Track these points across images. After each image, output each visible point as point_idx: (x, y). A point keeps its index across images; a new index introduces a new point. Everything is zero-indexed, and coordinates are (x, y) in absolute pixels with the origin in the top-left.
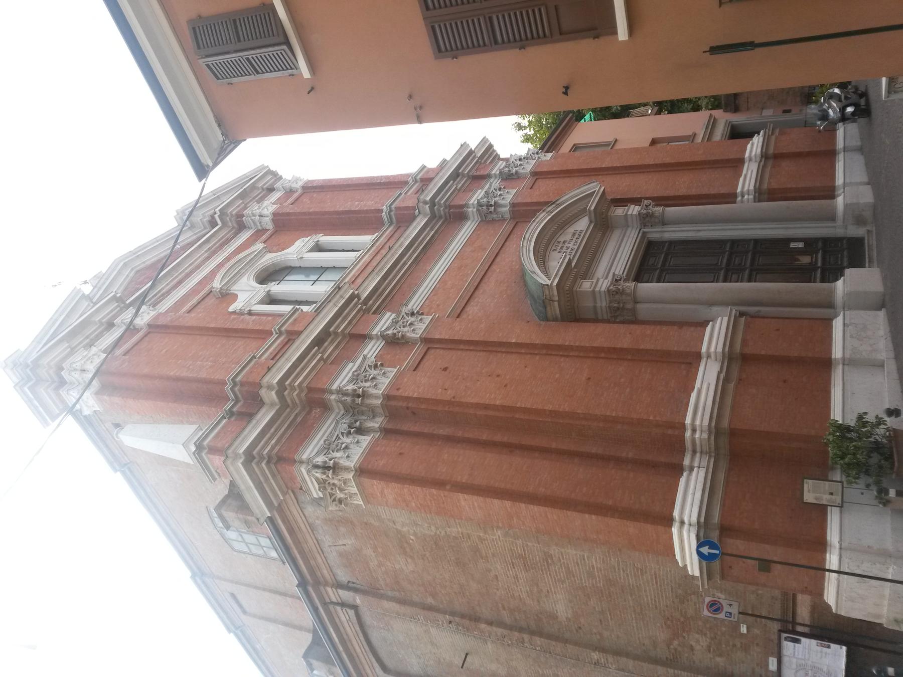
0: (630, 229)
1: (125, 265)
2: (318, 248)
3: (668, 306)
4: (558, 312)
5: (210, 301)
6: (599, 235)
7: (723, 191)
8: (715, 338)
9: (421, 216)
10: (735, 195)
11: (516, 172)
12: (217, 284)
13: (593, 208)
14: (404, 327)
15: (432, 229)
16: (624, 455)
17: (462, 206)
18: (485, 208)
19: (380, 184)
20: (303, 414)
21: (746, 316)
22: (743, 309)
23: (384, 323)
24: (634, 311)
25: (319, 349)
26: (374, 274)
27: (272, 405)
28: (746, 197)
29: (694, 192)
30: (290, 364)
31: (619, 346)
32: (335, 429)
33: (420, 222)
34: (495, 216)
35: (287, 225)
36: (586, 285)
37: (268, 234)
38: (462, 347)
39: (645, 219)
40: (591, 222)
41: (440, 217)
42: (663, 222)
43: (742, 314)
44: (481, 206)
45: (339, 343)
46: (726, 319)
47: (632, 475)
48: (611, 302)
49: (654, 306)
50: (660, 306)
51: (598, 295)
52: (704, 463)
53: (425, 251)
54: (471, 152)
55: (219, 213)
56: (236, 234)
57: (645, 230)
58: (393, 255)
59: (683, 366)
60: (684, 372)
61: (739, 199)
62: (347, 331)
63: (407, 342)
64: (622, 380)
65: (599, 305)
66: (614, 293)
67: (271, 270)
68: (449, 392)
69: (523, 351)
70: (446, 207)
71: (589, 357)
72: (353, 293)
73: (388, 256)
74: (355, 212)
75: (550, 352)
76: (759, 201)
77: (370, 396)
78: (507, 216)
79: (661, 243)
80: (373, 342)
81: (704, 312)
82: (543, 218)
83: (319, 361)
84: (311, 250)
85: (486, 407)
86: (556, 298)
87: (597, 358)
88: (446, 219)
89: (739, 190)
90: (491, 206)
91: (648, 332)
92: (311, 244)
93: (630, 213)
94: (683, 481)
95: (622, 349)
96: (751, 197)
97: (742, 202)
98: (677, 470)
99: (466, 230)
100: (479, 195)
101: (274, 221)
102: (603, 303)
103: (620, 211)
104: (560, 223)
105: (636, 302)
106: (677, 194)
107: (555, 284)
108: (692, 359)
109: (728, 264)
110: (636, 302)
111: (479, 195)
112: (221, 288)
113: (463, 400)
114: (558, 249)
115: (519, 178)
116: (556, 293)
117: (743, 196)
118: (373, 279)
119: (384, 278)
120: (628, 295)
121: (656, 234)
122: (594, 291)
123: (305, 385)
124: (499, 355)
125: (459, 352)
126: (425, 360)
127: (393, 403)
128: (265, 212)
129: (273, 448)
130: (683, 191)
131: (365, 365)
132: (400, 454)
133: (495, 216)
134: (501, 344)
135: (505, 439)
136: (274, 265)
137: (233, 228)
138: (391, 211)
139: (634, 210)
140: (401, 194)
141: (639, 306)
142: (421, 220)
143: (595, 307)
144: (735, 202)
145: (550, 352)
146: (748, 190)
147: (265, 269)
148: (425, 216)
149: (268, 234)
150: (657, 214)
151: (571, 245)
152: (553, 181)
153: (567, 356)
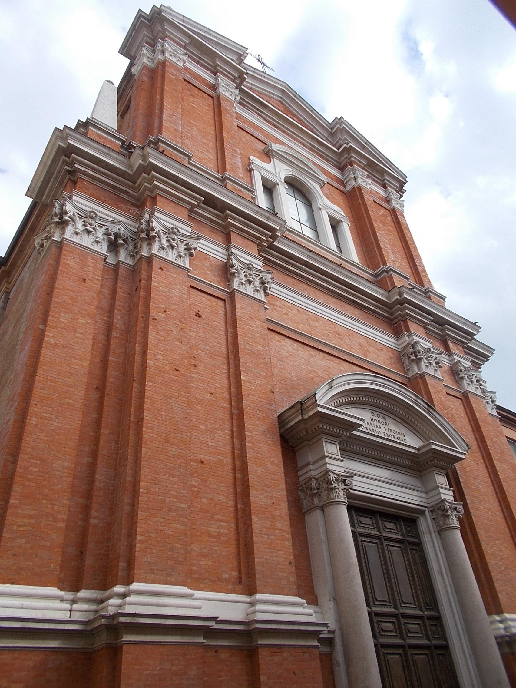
0: (424, 495)
1: (283, 92)
2: (335, 225)
3: (324, 547)
4: (292, 423)
5: (261, 147)
6: (407, 462)
7: (502, 597)
8: (280, 607)
9: (386, 293)
10: (500, 612)
11: (462, 378)
12: (275, 147)
13: (433, 447)
14: (246, 276)
15: (376, 306)
16: (94, 513)
17: (408, 330)
18: (412, 350)
19: (415, 266)
20: (132, 200)
21: (324, 648)
22: (338, 642)
23: (245, 256)
24: (312, 509)
25: (204, 203)
26: (308, 253)
27: (130, 167)
28: (502, 626)
29: (491, 562)
30: (177, 174)
31: (252, 492)
32: (111, 222)
33: (379, 293)
34: (407, 363)
35: (353, 199)
36: (331, 449)
37: (341, 188)
38: (230, 330)
39: (439, 510)
40: (418, 449)
41: (392, 314)
42: (440, 532)
43: (330, 642)
44: (413, 346)
45: (217, 223)
46: (312, 619)
47: (62, 525)
48: (316, 479)
49: (322, 530)
50: (323, 537)
51: (321, 463)
52: (77, 617)
53: (346, 295)
54: (472, 335)
55: (348, 146)
56: (336, 166)
57: (427, 512)
58: (334, 270)
59: (235, 574)
60: (225, 576)
61: (497, 618)
62: (232, 229)
63: (229, 281)
64: (204, 500)
65: (311, 467)
66: (325, 481)
67: (304, 190)
68: (163, 315)
69: (233, 389)
70: (402, 316)
71: (234, 461)
72: (276, 230)
73: (332, 265)
74: (376, 237)
75: (235, 417)
76: (499, 644)
77: (150, 245)
78: (410, 375)
79: (417, 534)
80: (224, 252)
81: (324, 592)
82: (407, 397)
83: (190, 203)
84: (331, 218)
85: (145, 353)
86: (306, 417)
87: (234, 469)
88: (392, 320)
89: (507, 615)
90: (416, 356)
91: (279, 525)
92: (337, 217)
93: (441, 490)
94: (54, 591)
95: (248, 495)
96: (503, 632)
97: (492, 623)
98: (73, 582)
99: (386, 339)
100: (424, 344)
101: (354, 189)
102: (314, 471)
103: (441, 480)
104: (405, 416)
105: (322, 508)
106: (482, 543)
107: (319, 409)
108: (247, 582)
109: (405, 616)
110: (322, 508)
111: (424, 344)
112: (272, 150)
113: (151, 327)
114: (374, 418)
115: (457, 382)
116: (311, 414)
117: (501, 622)
118: (301, 253)
119: (306, 264)
120: (328, 498)
121: (425, 524)
122: (324, 457)
123: (158, 192)
124: (225, 367)
125: (223, 329)
126: (209, 297)
127: (144, 266)
128: (360, 181)
129: (84, 173)
130: (487, 549)
131: (188, 240)
132: (84, 280)
133: (407, 363)
134: (237, 366)
135: (110, 380)
136: (309, 190)
137: (340, 163)
138: (387, 272)
139: (447, 495)
140: (407, 279)
141: (318, 512)
142: (382, 295)
143: (308, 464)
144: (489, 613)
145: (235, 417)
146: (510, 627)
147: (302, 184)
148: (388, 298)
149: (341, 188)
150: (449, 521)
151: (383, 430)
152: (463, 415)
153: (232, 437)
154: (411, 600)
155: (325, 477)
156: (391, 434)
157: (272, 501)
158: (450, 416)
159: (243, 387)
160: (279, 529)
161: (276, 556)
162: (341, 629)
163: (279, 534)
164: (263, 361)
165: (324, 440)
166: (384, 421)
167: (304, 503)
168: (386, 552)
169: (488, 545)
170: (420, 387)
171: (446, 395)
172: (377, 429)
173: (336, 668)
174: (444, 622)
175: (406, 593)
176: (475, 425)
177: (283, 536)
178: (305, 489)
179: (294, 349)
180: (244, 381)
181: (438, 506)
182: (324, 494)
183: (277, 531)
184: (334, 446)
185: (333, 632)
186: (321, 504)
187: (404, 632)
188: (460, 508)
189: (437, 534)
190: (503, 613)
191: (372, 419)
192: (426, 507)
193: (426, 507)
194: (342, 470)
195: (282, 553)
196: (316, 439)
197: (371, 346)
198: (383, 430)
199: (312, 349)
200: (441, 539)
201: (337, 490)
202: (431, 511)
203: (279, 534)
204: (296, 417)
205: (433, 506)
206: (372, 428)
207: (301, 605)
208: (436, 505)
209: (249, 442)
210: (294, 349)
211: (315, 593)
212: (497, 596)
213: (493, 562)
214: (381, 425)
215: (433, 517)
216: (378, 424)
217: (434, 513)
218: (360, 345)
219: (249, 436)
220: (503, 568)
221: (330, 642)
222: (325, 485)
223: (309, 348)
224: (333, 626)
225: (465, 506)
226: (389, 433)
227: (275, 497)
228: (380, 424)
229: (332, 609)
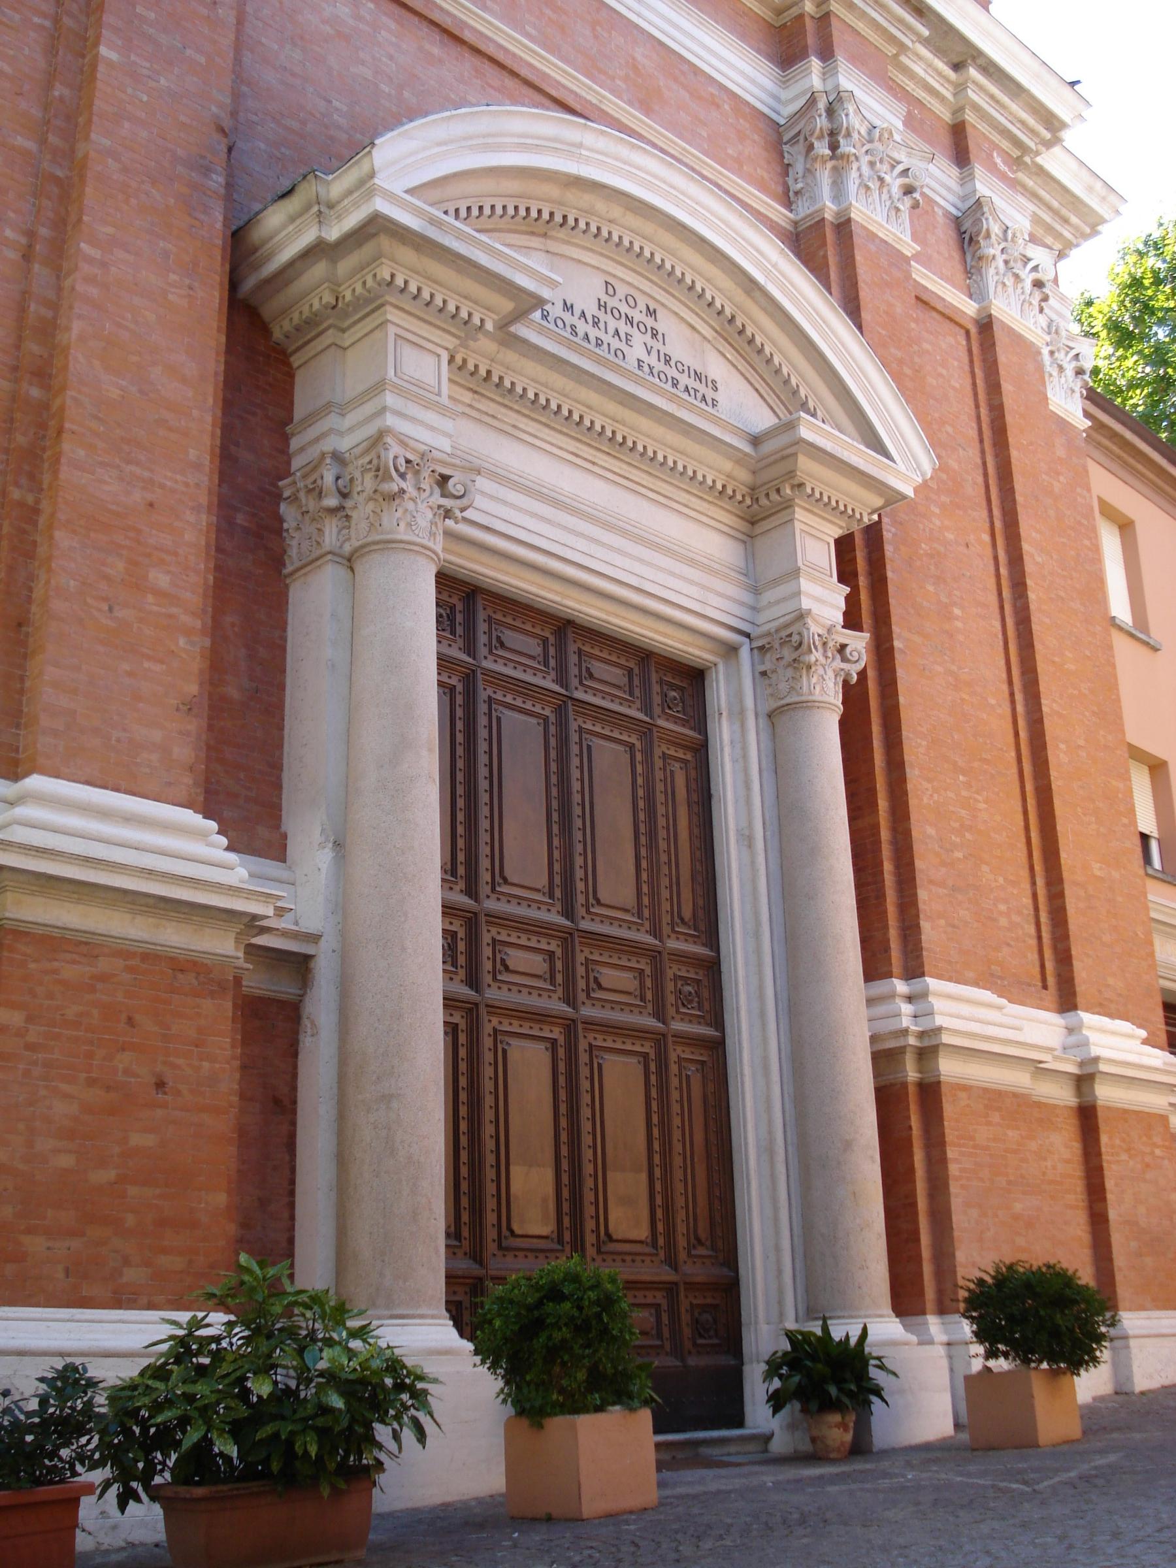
34: (799, 167)
51: (369, 408)
91: (160, 579)
105: (350, 562)
110: (350, 562)
121: (733, 699)
122: (379, 387)
154: (626, 895)
155: (373, 455)
156: (667, 369)
157: (150, 497)
158: (907, 371)
159: (99, 84)
160: (159, 593)
161: (130, 674)
162: (343, 934)
163: (155, 608)
164: (205, 12)
165: (392, 330)
166: (650, 322)
167: (294, 543)
168: (575, 749)
169: (929, 780)
170: (825, 257)
171: (913, 301)
172: (615, 343)
173: (306, 1042)
174: (724, 977)
175: (617, 879)
176: (992, 421)
177: (171, 616)
178: (302, 495)
179: (359, 18)
180: (110, 64)
181: (784, 634)
182: (361, 510)
183: (150, 598)
184: (430, 360)
185: (315, 938)
186: (347, 549)
187: (581, 984)
188: (859, 643)
189: (763, 721)
190: (923, 975)
191: (602, 306)
192: (748, 635)
193: (748, 635)
194: (445, 444)
195: (158, 668)
196: (369, 324)
197: (676, 80)
198: (637, 351)
199: (437, 36)
200: (774, 736)
201: (410, 506)
202: (761, 648)
203: (155, 608)
204: (299, 232)
205: (769, 634)
206: (593, 333)
207: (202, 835)
208: (778, 631)
209: (90, 280)
210: (359, 18)
211: (283, 828)
212: (918, 926)
213: (931, 831)
214: (634, 331)
215: (762, 668)
216: (624, 328)
217: (768, 655)
218: (635, 67)
219: (90, 260)
220: (959, 855)
221: (299, 966)
222: (369, 482)
223: (425, 29)
224: (312, 922)
225: (883, 651)
226: (659, 366)
227: (162, 486)
228: (628, 329)
229: (324, 871)
